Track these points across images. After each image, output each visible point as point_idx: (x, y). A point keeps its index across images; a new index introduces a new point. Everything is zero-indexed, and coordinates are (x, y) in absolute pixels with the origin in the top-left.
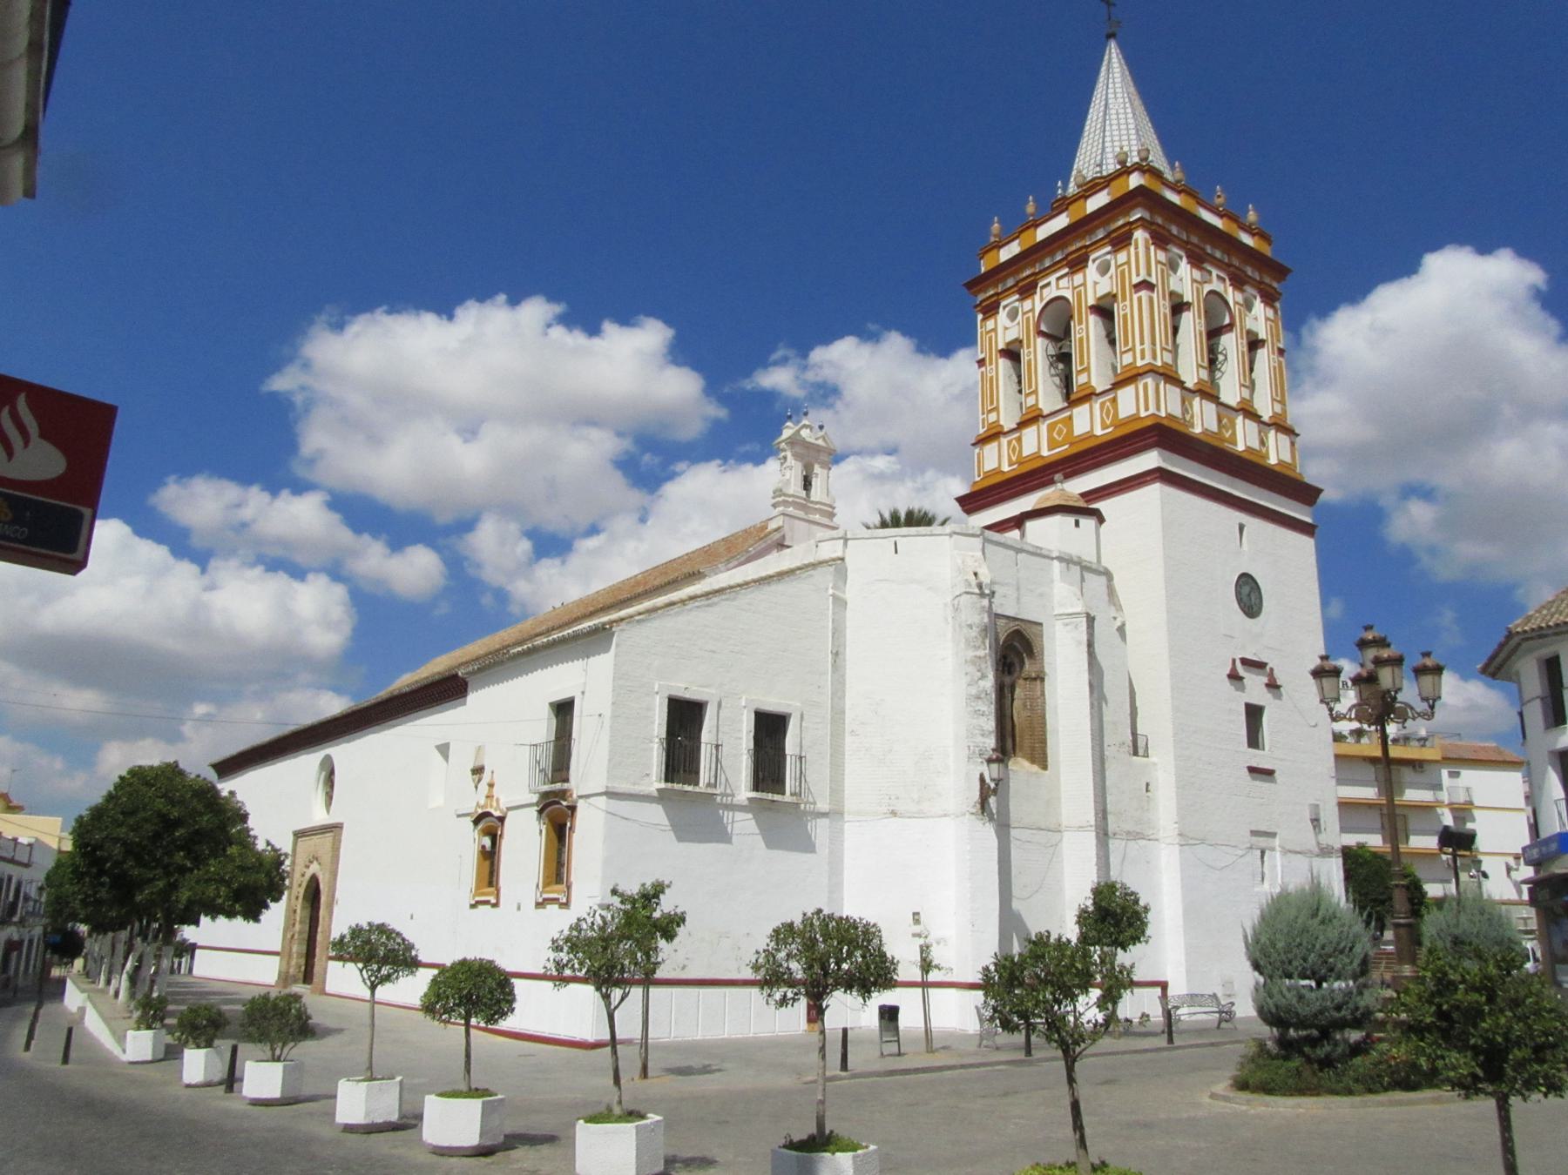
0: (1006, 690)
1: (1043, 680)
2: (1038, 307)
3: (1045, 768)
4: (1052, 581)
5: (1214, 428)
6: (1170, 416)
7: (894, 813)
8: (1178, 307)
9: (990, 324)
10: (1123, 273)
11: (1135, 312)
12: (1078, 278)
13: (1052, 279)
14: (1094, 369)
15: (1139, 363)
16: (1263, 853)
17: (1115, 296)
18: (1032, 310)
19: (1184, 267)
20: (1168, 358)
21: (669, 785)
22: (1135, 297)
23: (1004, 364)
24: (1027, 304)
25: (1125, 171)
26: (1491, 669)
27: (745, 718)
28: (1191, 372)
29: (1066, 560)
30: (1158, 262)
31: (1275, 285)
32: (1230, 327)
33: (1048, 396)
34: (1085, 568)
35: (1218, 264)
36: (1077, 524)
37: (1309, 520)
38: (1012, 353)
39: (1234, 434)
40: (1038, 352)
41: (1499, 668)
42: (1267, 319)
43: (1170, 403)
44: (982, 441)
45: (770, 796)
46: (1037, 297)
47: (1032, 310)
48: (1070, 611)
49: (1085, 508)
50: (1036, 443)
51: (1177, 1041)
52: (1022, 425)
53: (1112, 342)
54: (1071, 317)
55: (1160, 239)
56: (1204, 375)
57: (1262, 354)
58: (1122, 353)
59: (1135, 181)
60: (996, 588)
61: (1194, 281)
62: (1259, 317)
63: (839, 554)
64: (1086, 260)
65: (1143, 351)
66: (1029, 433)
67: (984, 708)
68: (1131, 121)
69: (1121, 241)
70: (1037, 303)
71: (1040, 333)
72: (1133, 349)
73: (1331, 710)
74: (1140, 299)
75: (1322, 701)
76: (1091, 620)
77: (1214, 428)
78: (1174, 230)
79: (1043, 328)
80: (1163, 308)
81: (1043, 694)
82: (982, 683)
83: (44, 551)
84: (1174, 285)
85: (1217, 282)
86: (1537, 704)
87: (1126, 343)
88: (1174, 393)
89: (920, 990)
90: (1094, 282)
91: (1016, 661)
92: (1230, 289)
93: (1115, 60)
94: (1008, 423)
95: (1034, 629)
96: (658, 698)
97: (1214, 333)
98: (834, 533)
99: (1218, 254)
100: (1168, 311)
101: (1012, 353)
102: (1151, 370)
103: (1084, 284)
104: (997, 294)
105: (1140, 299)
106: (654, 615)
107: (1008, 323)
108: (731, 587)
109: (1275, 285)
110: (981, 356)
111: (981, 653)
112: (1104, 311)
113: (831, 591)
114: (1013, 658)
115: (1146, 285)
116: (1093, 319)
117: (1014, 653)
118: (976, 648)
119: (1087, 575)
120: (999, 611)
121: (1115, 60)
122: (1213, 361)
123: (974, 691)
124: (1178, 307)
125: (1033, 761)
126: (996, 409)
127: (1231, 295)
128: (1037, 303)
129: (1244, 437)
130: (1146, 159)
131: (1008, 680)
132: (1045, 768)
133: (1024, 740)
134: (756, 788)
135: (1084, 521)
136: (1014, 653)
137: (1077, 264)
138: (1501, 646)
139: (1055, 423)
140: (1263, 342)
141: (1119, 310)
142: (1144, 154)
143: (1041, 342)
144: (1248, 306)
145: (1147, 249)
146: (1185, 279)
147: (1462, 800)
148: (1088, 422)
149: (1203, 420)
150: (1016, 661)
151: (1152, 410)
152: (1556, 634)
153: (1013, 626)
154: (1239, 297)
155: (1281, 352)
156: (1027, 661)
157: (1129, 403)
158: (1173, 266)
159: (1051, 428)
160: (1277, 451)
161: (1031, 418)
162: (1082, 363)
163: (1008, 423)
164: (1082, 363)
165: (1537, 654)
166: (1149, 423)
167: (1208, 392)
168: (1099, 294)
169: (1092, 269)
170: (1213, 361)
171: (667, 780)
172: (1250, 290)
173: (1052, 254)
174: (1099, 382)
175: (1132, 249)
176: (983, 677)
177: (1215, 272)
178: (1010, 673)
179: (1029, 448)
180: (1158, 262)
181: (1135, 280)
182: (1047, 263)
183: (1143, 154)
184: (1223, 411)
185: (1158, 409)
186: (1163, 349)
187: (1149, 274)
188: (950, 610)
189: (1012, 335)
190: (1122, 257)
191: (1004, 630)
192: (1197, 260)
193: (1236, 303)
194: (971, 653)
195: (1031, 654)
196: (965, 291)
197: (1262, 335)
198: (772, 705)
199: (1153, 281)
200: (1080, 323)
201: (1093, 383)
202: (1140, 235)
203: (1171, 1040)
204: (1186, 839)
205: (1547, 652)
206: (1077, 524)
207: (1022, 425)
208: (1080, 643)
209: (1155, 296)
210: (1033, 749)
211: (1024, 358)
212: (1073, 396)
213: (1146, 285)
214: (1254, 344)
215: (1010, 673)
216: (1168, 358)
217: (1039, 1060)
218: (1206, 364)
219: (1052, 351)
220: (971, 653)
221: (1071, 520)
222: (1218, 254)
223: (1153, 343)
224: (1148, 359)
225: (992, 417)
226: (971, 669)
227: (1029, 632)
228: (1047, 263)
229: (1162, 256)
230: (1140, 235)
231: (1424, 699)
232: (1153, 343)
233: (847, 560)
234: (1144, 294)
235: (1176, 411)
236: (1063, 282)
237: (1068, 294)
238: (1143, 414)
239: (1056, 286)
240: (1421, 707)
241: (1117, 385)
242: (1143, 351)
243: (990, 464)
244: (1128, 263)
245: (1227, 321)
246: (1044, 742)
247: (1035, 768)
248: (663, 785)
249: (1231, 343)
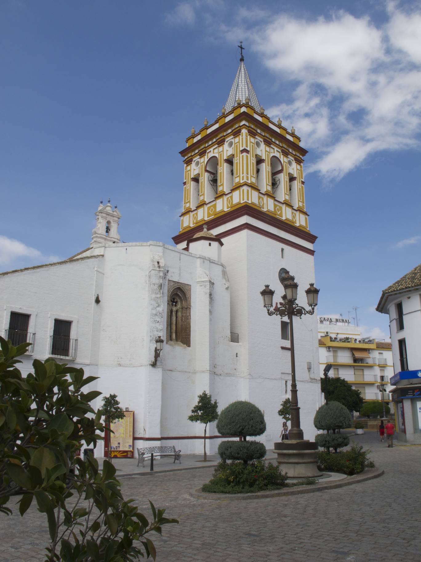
2: (206, 160)
3: (189, 346)
5: (273, 210)
6: (252, 203)
7: (120, 365)
8: (259, 161)
9: (189, 168)
10: (237, 146)
11: (245, 164)
12: (221, 149)
13: (212, 149)
14: (225, 185)
15: (242, 182)
16: (286, 382)
17: (233, 155)
18: (204, 162)
19: (263, 145)
20: (254, 180)
21: (54, 356)
22: (241, 155)
23: (193, 183)
24: (202, 160)
25: (240, 106)
26: (380, 309)
27: (49, 322)
28: (265, 186)
29: (203, 258)
30: (251, 142)
31: (301, 157)
32: (281, 171)
33: (207, 194)
34: (211, 261)
35: (277, 146)
36: (210, 244)
37: (312, 249)
38: (196, 180)
39: (282, 212)
40: (205, 178)
41: (382, 308)
42: (297, 169)
43: (254, 198)
44: (183, 214)
45: (62, 357)
46: (206, 157)
47: (204, 162)
49: (218, 239)
50: (203, 215)
51: (155, 469)
52: (198, 207)
53: (232, 174)
54: (218, 164)
55: (252, 133)
56: (269, 188)
57: (296, 184)
58: (236, 178)
59: (243, 109)
60: (169, 269)
61: (266, 151)
62: (294, 169)
63: (102, 254)
64: (224, 142)
65: (243, 177)
66: (201, 211)
68: (247, 91)
69: (237, 133)
70: (206, 159)
71: (206, 171)
72: (239, 176)
73: (268, 310)
74: (243, 156)
75: (265, 306)
76: (212, 284)
77: (273, 210)
78: (259, 131)
79: (208, 169)
80: (254, 161)
81: (190, 315)
82: (158, 309)
84: (259, 152)
85: (276, 152)
86: (394, 322)
87: (237, 174)
88: (255, 194)
89: (203, 440)
90: (226, 150)
91: (179, 300)
92: (282, 156)
93: (242, 69)
94: (193, 208)
96: (5, 312)
97: (274, 174)
98: (100, 245)
99: (277, 142)
100: (288, 180)
101: (196, 180)
102: (246, 184)
103: (223, 151)
104: (192, 156)
105: (243, 156)
106: (6, 276)
107: (195, 168)
108: (46, 265)
109: (301, 157)
110: (185, 181)
112: (230, 161)
113: (96, 269)
115: (245, 151)
116: (226, 165)
117: (178, 296)
118: (156, 294)
121: (242, 69)
122: (274, 184)
123: (154, 312)
124: (259, 161)
126: (189, 202)
127: (283, 159)
128: (206, 159)
129: (286, 214)
130: (248, 103)
134: (53, 352)
135: (213, 243)
136: (178, 296)
137: (221, 143)
138: (382, 298)
139: (211, 206)
140: (295, 178)
141: (235, 161)
142: (248, 99)
143: (206, 174)
144: (290, 163)
145: (246, 136)
146: (263, 151)
147: (383, 363)
148: (222, 206)
149: (268, 205)
151: (245, 200)
152: (400, 293)
153: (177, 286)
154: (286, 160)
155: (303, 183)
157: (237, 198)
158: (258, 144)
159: (209, 209)
160: (300, 221)
161: (202, 205)
162: (221, 182)
163: (193, 208)
164: (221, 182)
166: (243, 205)
167: (271, 195)
168: (228, 155)
169: (226, 145)
170: (274, 184)
171: (52, 354)
172: (259, 139)
173: (212, 139)
174: (226, 190)
175: (241, 136)
177: (276, 149)
179: (200, 217)
180: (251, 142)
181: (241, 149)
182: (210, 143)
183: (247, 101)
184: (276, 203)
185: (248, 200)
186: (251, 176)
187: (247, 147)
188: (147, 278)
189: (196, 172)
190: (237, 140)
192: (268, 143)
193: (284, 162)
194: (154, 296)
196: (180, 155)
197: (295, 176)
198: (64, 317)
199: (248, 149)
200: (221, 166)
201: (225, 190)
202: (244, 131)
203: (152, 469)
204: (251, 376)
205: (397, 301)
206: (210, 244)
207: (198, 207)
209: (249, 155)
211: (200, 181)
212: (219, 196)
213: (245, 151)
214: (292, 179)
216: (287, 197)
217: (157, 472)
218: (270, 184)
219: (210, 179)
220: (154, 296)
221: (207, 242)
222: (277, 142)
223: (247, 174)
224: (245, 180)
225: (188, 205)
226: (153, 302)
228: (210, 143)
229: (252, 140)
230: (244, 131)
231: (311, 305)
232: (247, 174)
233: (106, 256)
234: (245, 154)
235: (290, 217)
236: (216, 151)
237: (217, 155)
238: (242, 202)
239: (213, 152)
240: (308, 308)
241: (233, 190)
242: (243, 177)
243: (186, 224)
244: (239, 142)
245: (280, 168)
248: (51, 356)
249: (283, 178)
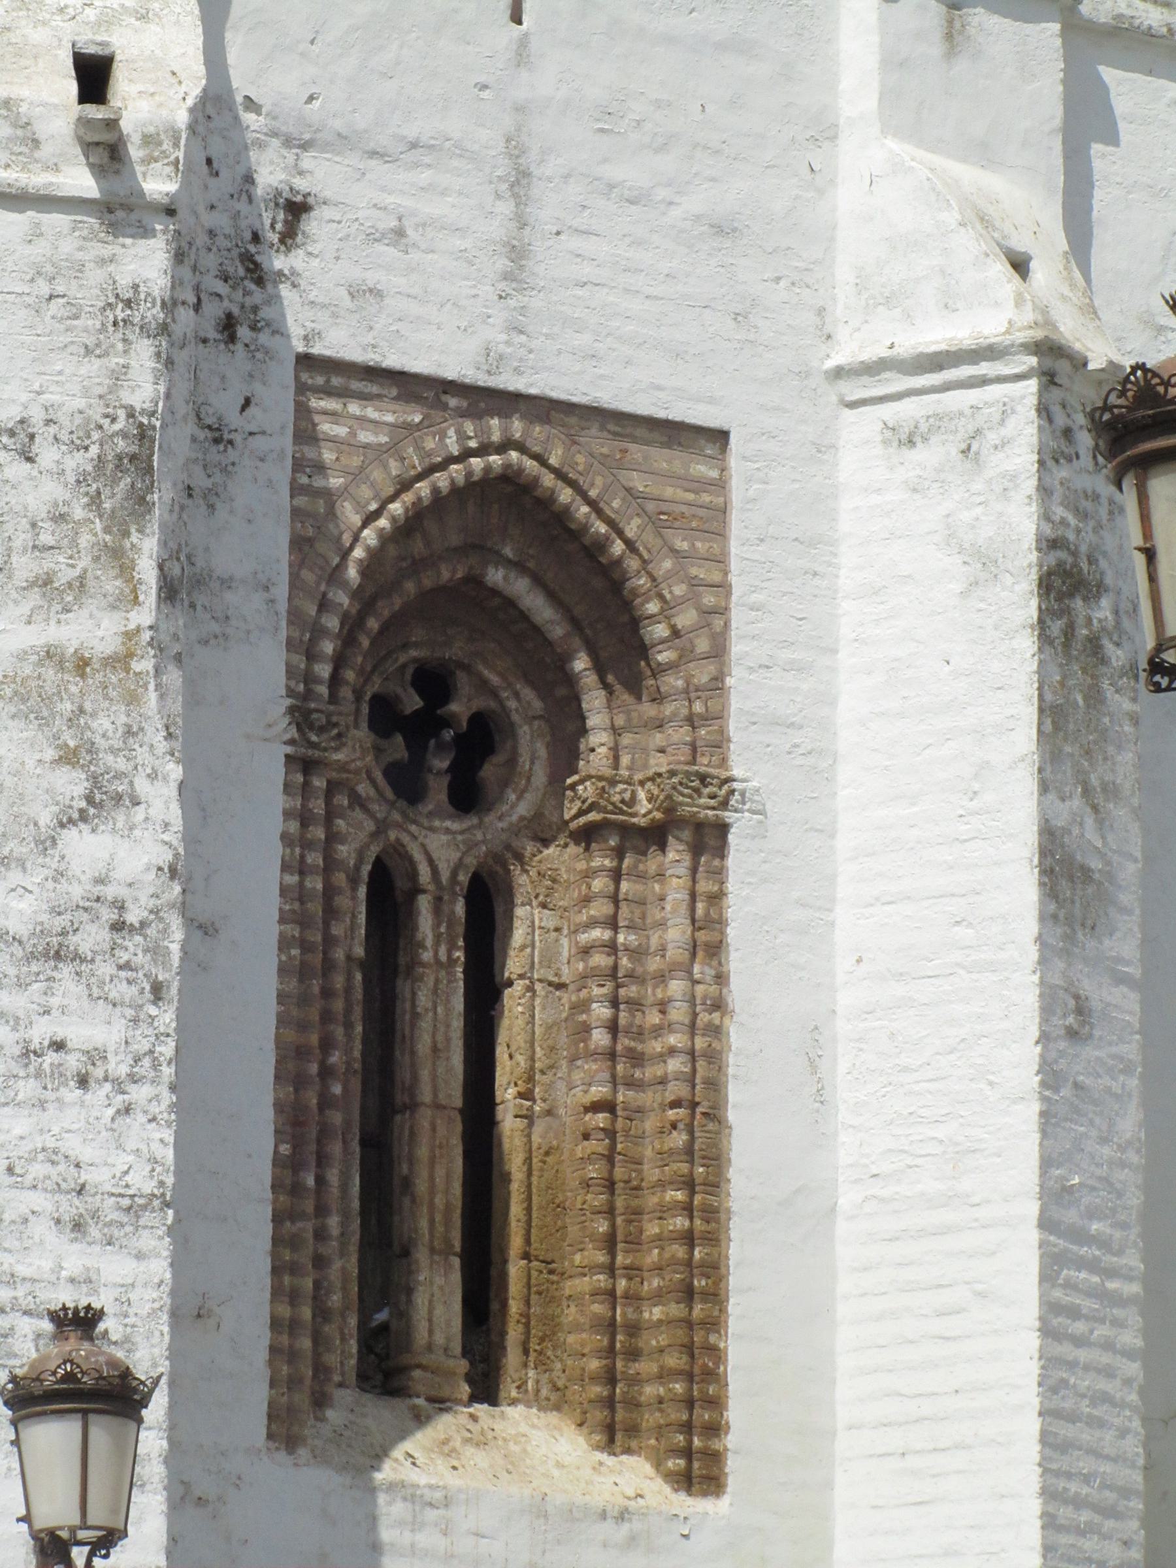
0: (435, 935)
1: (709, 839)
3: (700, 1472)
4: (825, 132)
48: (936, 335)
67: (93, 1029)
81: (708, 941)
82: (86, 848)
83: (38, 1409)
91: (522, 703)
95: (654, 471)
111: (95, 629)
114: (491, 683)
119: (1127, 89)
120: (341, 342)
125: (614, 1431)
131: (440, 846)
132: (700, 1472)
133: (563, 1279)
150: (522, 703)
156: (595, 705)
165: (241, 113)
176: (102, 802)
178: (467, 797)
191: (373, 475)
195: (627, 657)
208: (986, 564)
210: (620, 1341)
215: (467, 797)
227: (611, 496)
246: (700, 1287)
247: (634, 1477)
